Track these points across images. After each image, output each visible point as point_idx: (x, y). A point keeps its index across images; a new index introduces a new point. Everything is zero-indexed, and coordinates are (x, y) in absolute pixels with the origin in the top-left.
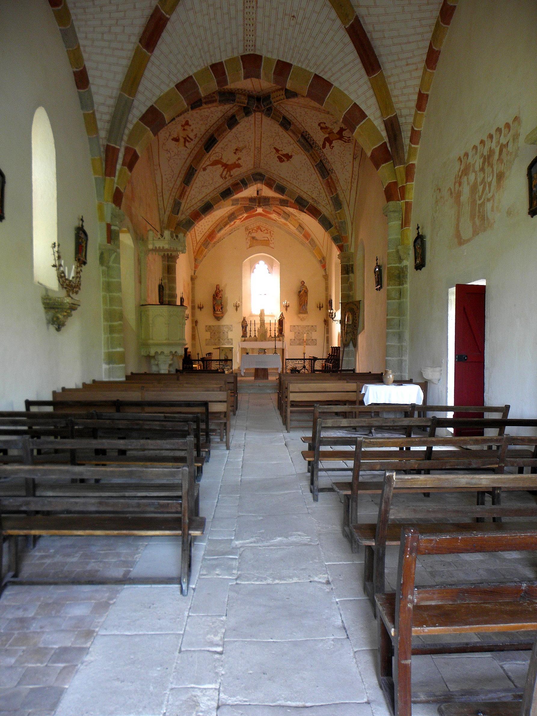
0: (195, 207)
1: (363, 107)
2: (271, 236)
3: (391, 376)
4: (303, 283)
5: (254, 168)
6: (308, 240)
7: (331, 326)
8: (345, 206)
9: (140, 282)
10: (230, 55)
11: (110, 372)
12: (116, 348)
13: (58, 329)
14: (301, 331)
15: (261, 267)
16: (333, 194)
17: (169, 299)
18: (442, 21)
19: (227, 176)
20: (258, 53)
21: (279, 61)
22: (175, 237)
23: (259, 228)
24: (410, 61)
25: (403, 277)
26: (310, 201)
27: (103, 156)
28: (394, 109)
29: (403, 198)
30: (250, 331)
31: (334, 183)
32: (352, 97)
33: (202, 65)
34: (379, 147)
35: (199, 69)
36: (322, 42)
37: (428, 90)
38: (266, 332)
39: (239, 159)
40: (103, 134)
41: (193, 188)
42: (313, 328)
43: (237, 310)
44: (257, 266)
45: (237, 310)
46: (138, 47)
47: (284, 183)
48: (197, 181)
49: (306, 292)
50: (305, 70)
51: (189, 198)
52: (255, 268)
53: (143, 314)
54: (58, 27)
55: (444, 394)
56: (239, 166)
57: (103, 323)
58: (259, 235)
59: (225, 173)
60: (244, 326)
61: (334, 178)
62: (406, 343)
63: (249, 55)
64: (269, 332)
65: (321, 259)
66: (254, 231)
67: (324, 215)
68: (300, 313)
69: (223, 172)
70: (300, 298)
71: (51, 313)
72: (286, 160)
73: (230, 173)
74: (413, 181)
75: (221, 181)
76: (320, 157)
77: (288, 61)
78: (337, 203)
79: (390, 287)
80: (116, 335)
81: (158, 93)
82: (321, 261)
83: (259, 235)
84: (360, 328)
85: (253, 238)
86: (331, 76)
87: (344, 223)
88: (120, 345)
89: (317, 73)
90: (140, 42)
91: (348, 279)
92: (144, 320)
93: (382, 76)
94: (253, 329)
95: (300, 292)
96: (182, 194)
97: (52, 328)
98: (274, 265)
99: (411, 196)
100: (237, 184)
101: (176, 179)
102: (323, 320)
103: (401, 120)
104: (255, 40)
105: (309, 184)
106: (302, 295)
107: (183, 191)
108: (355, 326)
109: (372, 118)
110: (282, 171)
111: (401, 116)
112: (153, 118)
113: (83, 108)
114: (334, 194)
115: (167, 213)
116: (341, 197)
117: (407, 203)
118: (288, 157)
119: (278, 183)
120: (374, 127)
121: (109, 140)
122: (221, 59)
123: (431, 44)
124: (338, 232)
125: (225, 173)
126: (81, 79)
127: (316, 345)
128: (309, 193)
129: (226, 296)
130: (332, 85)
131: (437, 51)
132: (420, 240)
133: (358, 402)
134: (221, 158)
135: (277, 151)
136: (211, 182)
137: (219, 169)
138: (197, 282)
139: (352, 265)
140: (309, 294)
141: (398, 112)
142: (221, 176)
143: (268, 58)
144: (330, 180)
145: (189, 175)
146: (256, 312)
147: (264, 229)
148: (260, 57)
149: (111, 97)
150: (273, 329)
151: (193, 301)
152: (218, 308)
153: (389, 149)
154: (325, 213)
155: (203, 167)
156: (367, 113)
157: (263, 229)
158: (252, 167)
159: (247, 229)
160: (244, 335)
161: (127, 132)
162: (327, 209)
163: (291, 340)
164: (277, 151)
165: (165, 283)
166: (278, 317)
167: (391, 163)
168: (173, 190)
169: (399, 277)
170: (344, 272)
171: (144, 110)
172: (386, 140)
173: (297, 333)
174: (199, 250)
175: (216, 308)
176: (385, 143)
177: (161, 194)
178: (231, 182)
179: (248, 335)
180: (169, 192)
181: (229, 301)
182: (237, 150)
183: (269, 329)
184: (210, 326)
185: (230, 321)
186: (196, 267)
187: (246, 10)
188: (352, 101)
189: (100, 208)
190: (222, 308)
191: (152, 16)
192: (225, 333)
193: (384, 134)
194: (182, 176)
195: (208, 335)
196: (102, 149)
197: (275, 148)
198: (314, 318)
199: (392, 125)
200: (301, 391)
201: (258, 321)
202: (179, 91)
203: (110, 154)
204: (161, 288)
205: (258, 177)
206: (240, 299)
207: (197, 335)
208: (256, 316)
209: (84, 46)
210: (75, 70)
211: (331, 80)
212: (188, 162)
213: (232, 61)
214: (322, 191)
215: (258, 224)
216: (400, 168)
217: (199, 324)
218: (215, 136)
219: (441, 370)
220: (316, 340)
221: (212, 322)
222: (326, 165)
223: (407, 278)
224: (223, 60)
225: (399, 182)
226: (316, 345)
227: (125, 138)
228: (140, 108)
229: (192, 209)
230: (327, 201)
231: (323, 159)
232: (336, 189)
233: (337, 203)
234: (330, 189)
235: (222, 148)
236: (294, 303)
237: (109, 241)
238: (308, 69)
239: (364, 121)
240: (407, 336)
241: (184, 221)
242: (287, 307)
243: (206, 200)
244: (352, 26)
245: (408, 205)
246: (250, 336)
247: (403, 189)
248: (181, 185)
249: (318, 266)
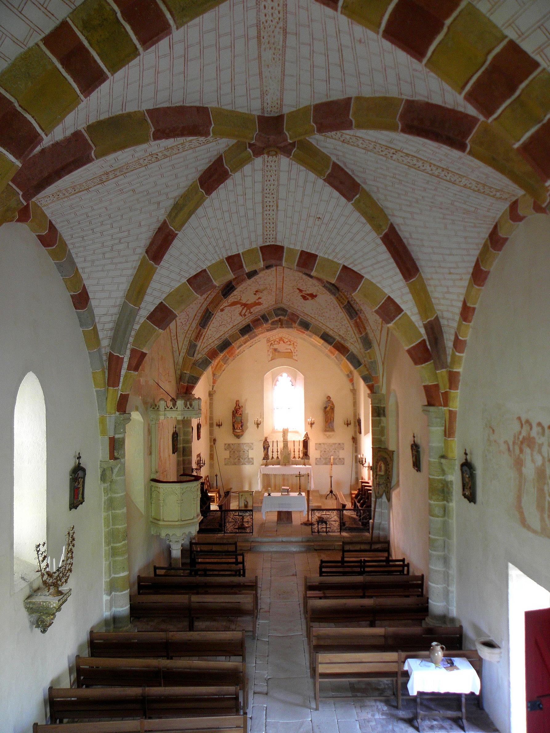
0: (212, 345)
1: (398, 301)
2: (295, 348)
3: (440, 653)
4: (329, 397)
5: (276, 303)
6: (334, 355)
7: (360, 443)
8: (375, 345)
9: (151, 454)
10: (248, 247)
11: (111, 603)
12: (119, 573)
13: (44, 631)
14: (328, 449)
15: (284, 379)
16: (361, 334)
17: (184, 445)
18: (491, 247)
19: (247, 313)
20: (279, 244)
21: (303, 252)
22: (189, 406)
23: (281, 339)
24: (452, 271)
25: (448, 493)
26: (337, 338)
27: (106, 364)
28: (435, 310)
29: (446, 405)
30: (273, 452)
31: (363, 324)
32: (387, 291)
33: (217, 258)
34: (417, 345)
35: (213, 262)
36: (352, 240)
37: (475, 304)
38: (289, 454)
39: (260, 298)
40: (105, 343)
41: (210, 328)
42: (340, 446)
43: (258, 427)
44: (280, 378)
45: (258, 427)
46: (144, 257)
47: (308, 319)
48: (214, 321)
49: (332, 409)
50: (332, 261)
51: (206, 338)
52: (277, 380)
53: (153, 489)
54: (53, 262)
55: (506, 684)
56: (259, 304)
57: (104, 548)
58: (282, 347)
59: (244, 311)
60: (266, 447)
61: (362, 318)
62: (453, 572)
63: (268, 246)
64: (292, 453)
65: (348, 373)
66: (276, 343)
67: (352, 352)
68: (326, 431)
69: (242, 311)
70: (327, 414)
71: (35, 616)
72: (310, 298)
73: (250, 311)
74: (457, 389)
75: (240, 319)
76: (347, 298)
77: (313, 252)
78: (367, 343)
79: (432, 502)
80: (119, 558)
81: (168, 290)
82: (348, 375)
83: (282, 347)
84: (394, 482)
85: (275, 350)
86: (362, 269)
87: (375, 362)
88: (123, 570)
89: (346, 264)
90: (147, 252)
91: (379, 422)
92: (154, 496)
93: (421, 280)
94: (275, 450)
95: (326, 408)
96: (198, 336)
97: (38, 631)
98: (298, 378)
99: (456, 405)
100: (258, 320)
101: (191, 322)
102: (351, 437)
103: (443, 322)
104: (276, 234)
105: (338, 322)
106: (328, 410)
107: (199, 333)
108: (388, 478)
109: (409, 313)
110: (307, 309)
111: (443, 318)
112: (162, 316)
113: (82, 325)
114: (364, 334)
115: (182, 354)
116: (371, 336)
117: (450, 411)
118: (313, 296)
119: (301, 319)
120: (411, 323)
121: (112, 348)
122: (238, 251)
123: (477, 261)
124: (368, 370)
125: (244, 311)
126: (81, 300)
127: (343, 464)
128: (336, 330)
129: (246, 412)
130: (362, 277)
131: (486, 272)
132: (467, 467)
133: (399, 674)
134: (240, 300)
135: (301, 291)
136: (229, 321)
137: (238, 308)
138: (215, 397)
139: (384, 408)
140: (336, 410)
141: (439, 313)
142: (240, 314)
143: (290, 249)
144: (358, 320)
145: (205, 318)
146: (279, 427)
147: (287, 340)
148: (282, 248)
149: (114, 306)
150: (297, 451)
151: (211, 418)
152: (238, 426)
153: (429, 347)
154: (353, 351)
155: (221, 308)
156: (403, 307)
157: (286, 340)
158: (274, 303)
159: (268, 341)
160: (266, 457)
161: (133, 333)
162: (355, 347)
163: (316, 459)
164: (301, 291)
165: (179, 429)
166: (302, 438)
167: (431, 363)
168: (189, 332)
169: (443, 491)
170: (375, 414)
171: (152, 308)
172: (425, 337)
173: (323, 452)
174: (217, 365)
175: (236, 426)
176: (424, 341)
177: (175, 337)
178: (251, 318)
179: (270, 457)
180: (184, 334)
181: (249, 418)
182: (257, 291)
183: (292, 451)
184: (229, 445)
185: (251, 439)
186: (214, 382)
187: (265, 212)
188: (386, 294)
189: (102, 421)
190: (242, 426)
191: (160, 229)
192: (246, 451)
193: (423, 331)
194: (198, 319)
195: (227, 454)
196: (105, 358)
197: (298, 289)
198: (341, 435)
199: (432, 328)
200: (332, 661)
201: (281, 445)
202: (191, 286)
203: (114, 363)
204: (175, 436)
205: (280, 312)
206: (262, 415)
207: (215, 454)
208: (279, 432)
209: (83, 268)
210: (72, 293)
211: (362, 272)
212: (204, 306)
213: (250, 252)
214: (350, 329)
215: (280, 335)
216: (443, 372)
217: (217, 443)
218: (234, 283)
219: (501, 653)
220: (343, 459)
221: (232, 440)
222: (354, 306)
223: (452, 495)
224: (240, 252)
225: (441, 386)
226: (343, 464)
227: (131, 340)
228: (149, 305)
229: (209, 347)
230: (355, 339)
231: (350, 300)
232: (365, 329)
233: (367, 343)
234: (359, 329)
235: (241, 291)
236: (319, 419)
237: (113, 457)
238: (335, 260)
239: (400, 316)
240: (454, 562)
241: (200, 360)
242: (312, 424)
243: (224, 338)
244: (386, 235)
245: (452, 415)
246: (273, 458)
247: (446, 395)
248: (197, 328)
249: (345, 380)
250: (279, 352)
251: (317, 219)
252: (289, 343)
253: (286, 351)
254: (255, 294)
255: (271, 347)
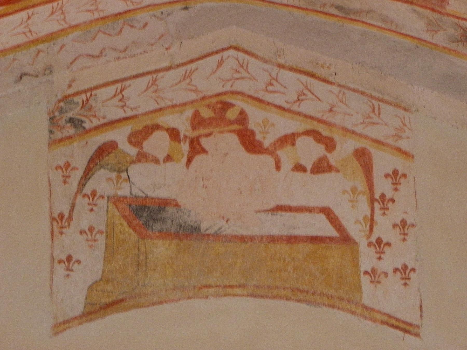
66: (158, 143)
83: (224, 190)
85: (147, 213)
147: (285, 125)
157: (270, 126)
250: (189, 233)
251: (60, 269)
252: (309, 151)
253: (277, 225)
254: (81, 233)
255: (102, 182)
